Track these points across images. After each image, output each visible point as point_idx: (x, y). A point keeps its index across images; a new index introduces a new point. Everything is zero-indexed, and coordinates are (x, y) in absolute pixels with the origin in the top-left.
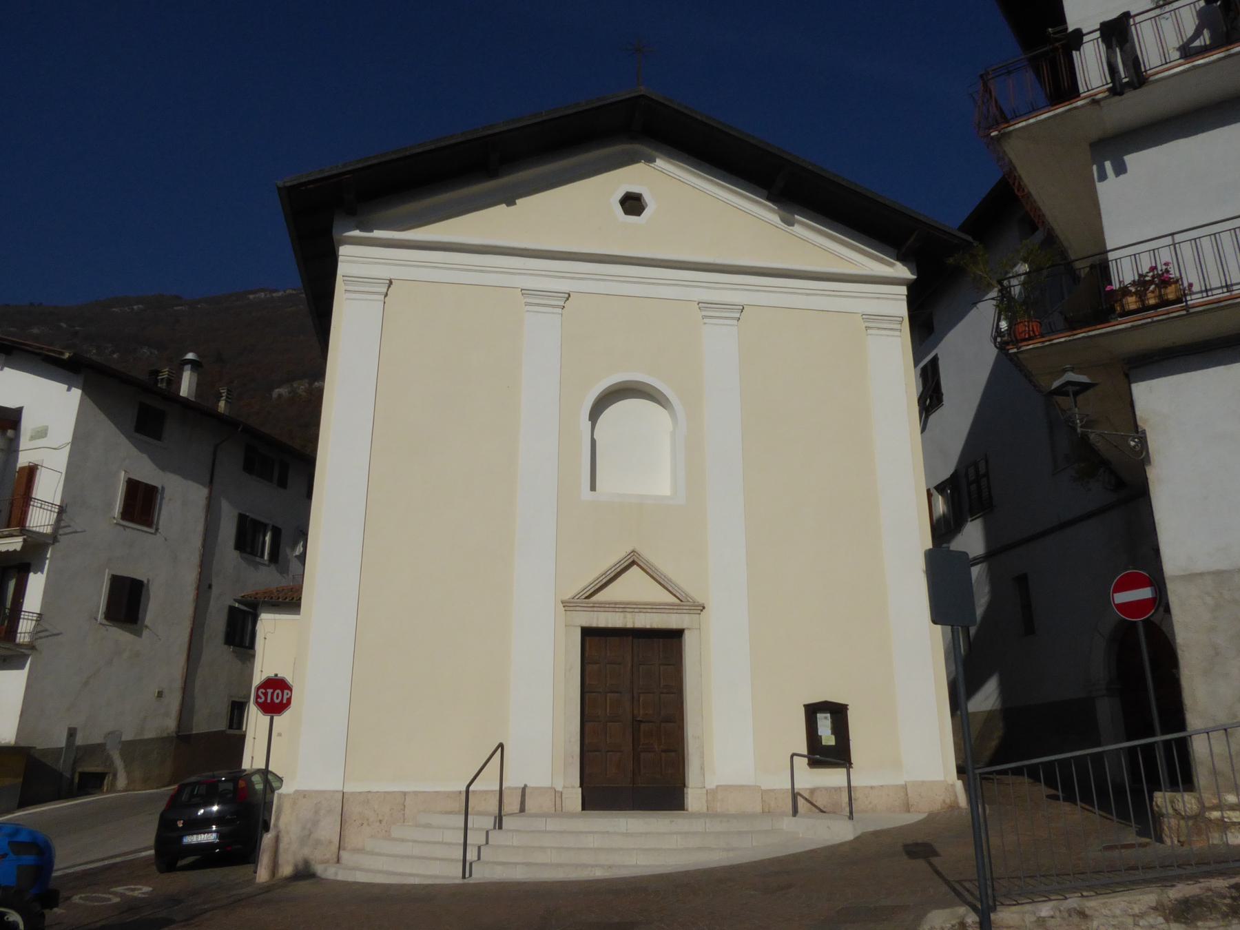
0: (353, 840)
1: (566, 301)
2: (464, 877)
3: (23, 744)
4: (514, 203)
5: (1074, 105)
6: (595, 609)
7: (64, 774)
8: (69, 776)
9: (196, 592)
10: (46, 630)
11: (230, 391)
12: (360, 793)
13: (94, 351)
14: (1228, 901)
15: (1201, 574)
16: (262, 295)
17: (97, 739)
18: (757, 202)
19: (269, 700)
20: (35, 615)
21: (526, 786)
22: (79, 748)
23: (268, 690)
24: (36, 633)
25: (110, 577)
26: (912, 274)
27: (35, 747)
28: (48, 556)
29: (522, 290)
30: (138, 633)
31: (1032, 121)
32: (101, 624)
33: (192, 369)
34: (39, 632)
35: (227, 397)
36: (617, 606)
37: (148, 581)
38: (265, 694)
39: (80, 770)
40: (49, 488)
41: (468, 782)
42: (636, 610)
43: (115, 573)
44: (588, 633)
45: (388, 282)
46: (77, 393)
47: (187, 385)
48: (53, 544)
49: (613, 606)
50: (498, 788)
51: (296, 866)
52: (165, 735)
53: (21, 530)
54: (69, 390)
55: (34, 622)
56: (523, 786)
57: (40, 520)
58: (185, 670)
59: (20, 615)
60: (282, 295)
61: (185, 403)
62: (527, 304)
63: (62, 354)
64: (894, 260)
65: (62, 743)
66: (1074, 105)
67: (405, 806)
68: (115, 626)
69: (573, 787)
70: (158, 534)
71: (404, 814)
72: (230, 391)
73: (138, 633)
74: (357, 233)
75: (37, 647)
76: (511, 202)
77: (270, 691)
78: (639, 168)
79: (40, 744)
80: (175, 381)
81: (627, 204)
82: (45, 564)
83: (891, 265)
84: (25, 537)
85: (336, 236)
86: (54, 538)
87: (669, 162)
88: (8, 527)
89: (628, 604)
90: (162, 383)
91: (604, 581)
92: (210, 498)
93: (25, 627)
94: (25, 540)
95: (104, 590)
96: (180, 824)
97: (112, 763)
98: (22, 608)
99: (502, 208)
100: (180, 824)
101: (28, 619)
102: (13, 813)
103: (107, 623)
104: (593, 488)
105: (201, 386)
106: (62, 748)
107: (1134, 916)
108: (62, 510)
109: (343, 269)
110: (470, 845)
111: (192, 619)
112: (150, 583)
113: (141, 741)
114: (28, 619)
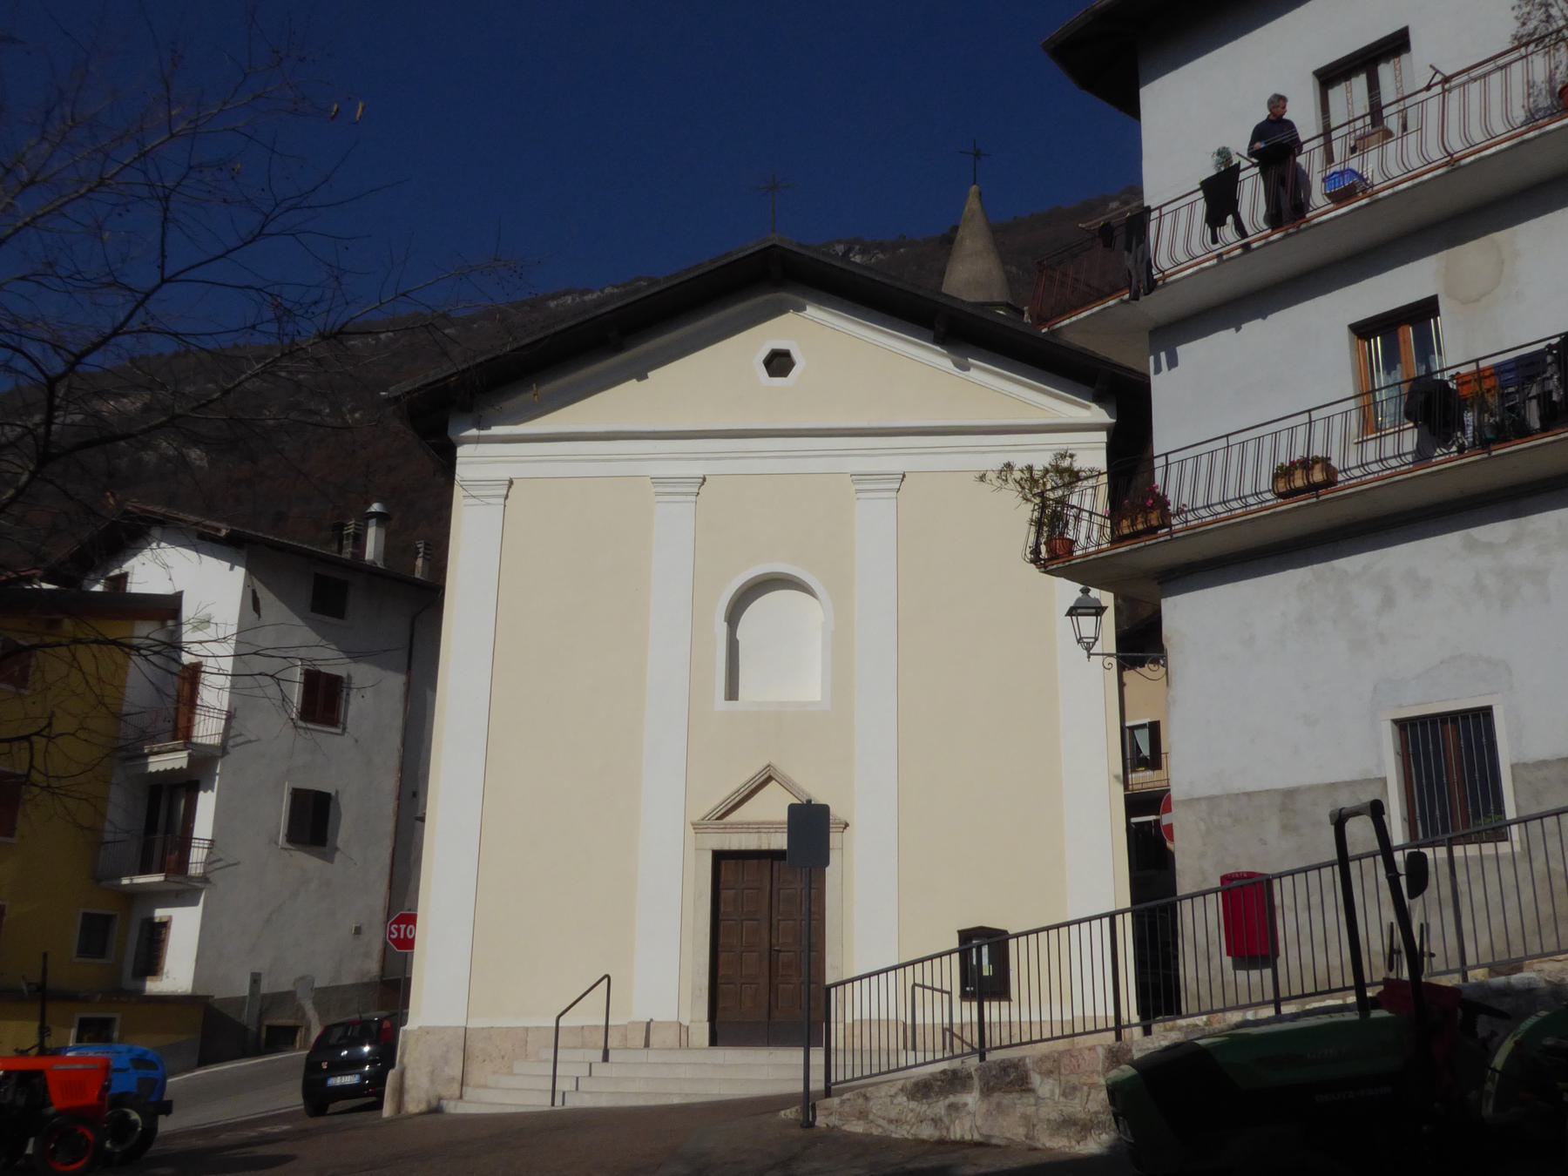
0: (475, 1076)
1: (700, 486)
2: (553, 1104)
3: (200, 993)
4: (646, 377)
5: (1106, 305)
6: (727, 830)
7: (250, 1027)
8: (254, 1029)
9: (397, 802)
10: (220, 860)
11: (429, 545)
12: (483, 1029)
13: (327, 411)
14: (939, 1083)
15: (1198, 799)
16: (569, 299)
17: (285, 986)
18: (923, 346)
19: (402, 936)
20: (206, 842)
21: (652, 1020)
22: (265, 996)
23: (401, 926)
24: (208, 863)
25: (291, 790)
26: (1111, 418)
27: (212, 997)
28: (218, 771)
29: (651, 478)
30: (329, 858)
31: (1074, 319)
32: (282, 848)
33: (378, 525)
34: (214, 862)
35: (425, 553)
36: (751, 826)
37: (337, 792)
38: (398, 930)
39: (267, 1022)
40: (214, 695)
41: (559, 1013)
42: (772, 830)
43: (298, 786)
44: (719, 857)
45: (507, 482)
46: (240, 572)
47: (373, 544)
48: (222, 757)
49: (746, 826)
50: (604, 1023)
51: (429, 1102)
52: (366, 980)
53: (185, 744)
54: (232, 569)
55: (206, 851)
56: (648, 1020)
57: (208, 730)
58: (387, 900)
59: (191, 843)
60: (599, 297)
61: (371, 571)
62: (658, 494)
63: (218, 530)
64: (1090, 402)
65: (244, 990)
66: (1106, 305)
67: (527, 1042)
68: (299, 850)
69: (700, 1021)
70: (346, 735)
71: (526, 1050)
72: (429, 545)
73: (329, 858)
74: (474, 432)
75: (211, 879)
76: (642, 376)
77: (403, 927)
78: (789, 318)
79: (220, 992)
80: (359, 540)
81: (775, 363)
82: (214, 780)
83: (1088, 407)
84: (190, 751)
85: (452, 435)
86: (223, 749)
87: (820, 309)
88: (174, 740)
89: (763, 823)
90: (348, 539)
91: (737, 799)
92: (408, 685)
93: (197, 855)
94: (189, 755)
95: (284, 808)
96: (325, 1066)
97: (304, 1015)
98: (192, 834)
99: (633, 384)
100: (325, 1066)
101: (199, 847)
102: (193, 1072)
103: (290, 847)
104: (732, 693)
105: (390, 548)
106: (244, 997)
107: (890, 1096)
108: (230, 717)
109: (463, 471)
110: (560, 1076)
111: (393, 836)
112: (340, 796)
113: (338, 987)
114: (199, 847)
